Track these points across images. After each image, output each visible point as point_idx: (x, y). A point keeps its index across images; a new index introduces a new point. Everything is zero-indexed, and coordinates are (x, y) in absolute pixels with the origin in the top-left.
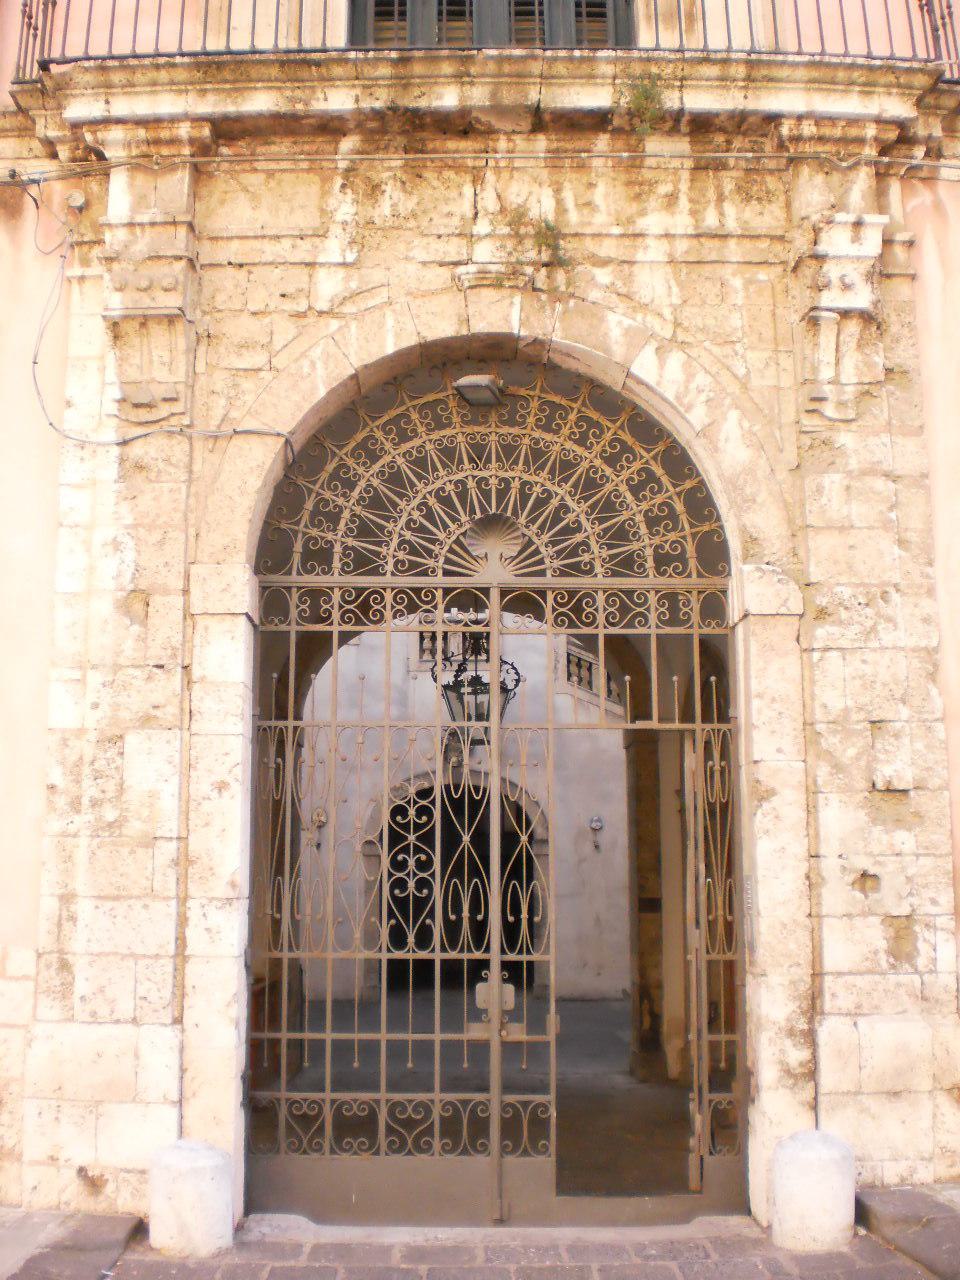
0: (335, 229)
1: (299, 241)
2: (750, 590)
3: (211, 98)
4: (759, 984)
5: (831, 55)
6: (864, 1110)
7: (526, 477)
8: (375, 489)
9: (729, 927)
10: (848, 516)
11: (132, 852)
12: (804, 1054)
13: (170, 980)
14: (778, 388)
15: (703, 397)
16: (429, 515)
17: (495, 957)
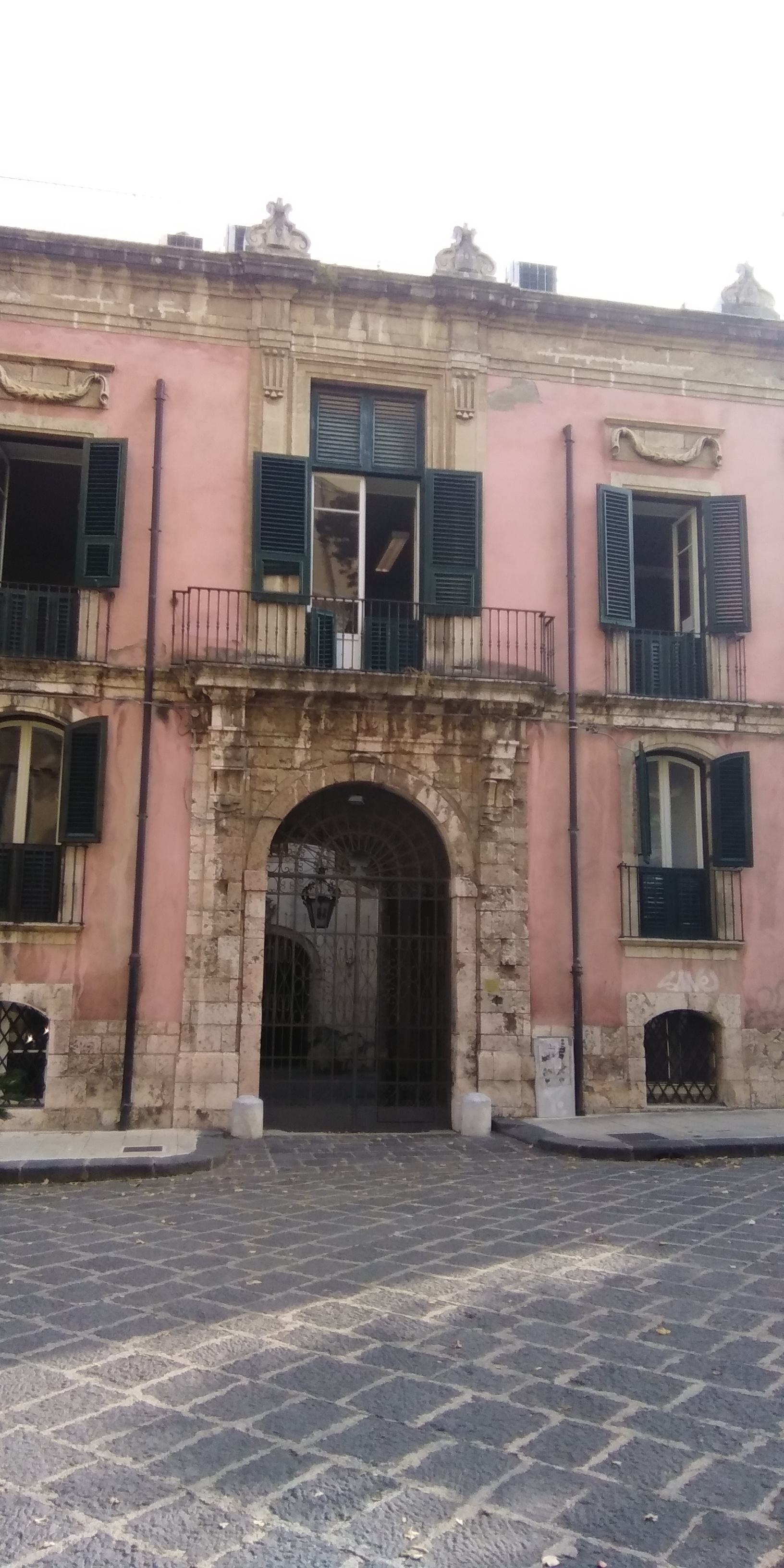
2: (459, 887)
6: (495, 1087)
12: (473, 1065)
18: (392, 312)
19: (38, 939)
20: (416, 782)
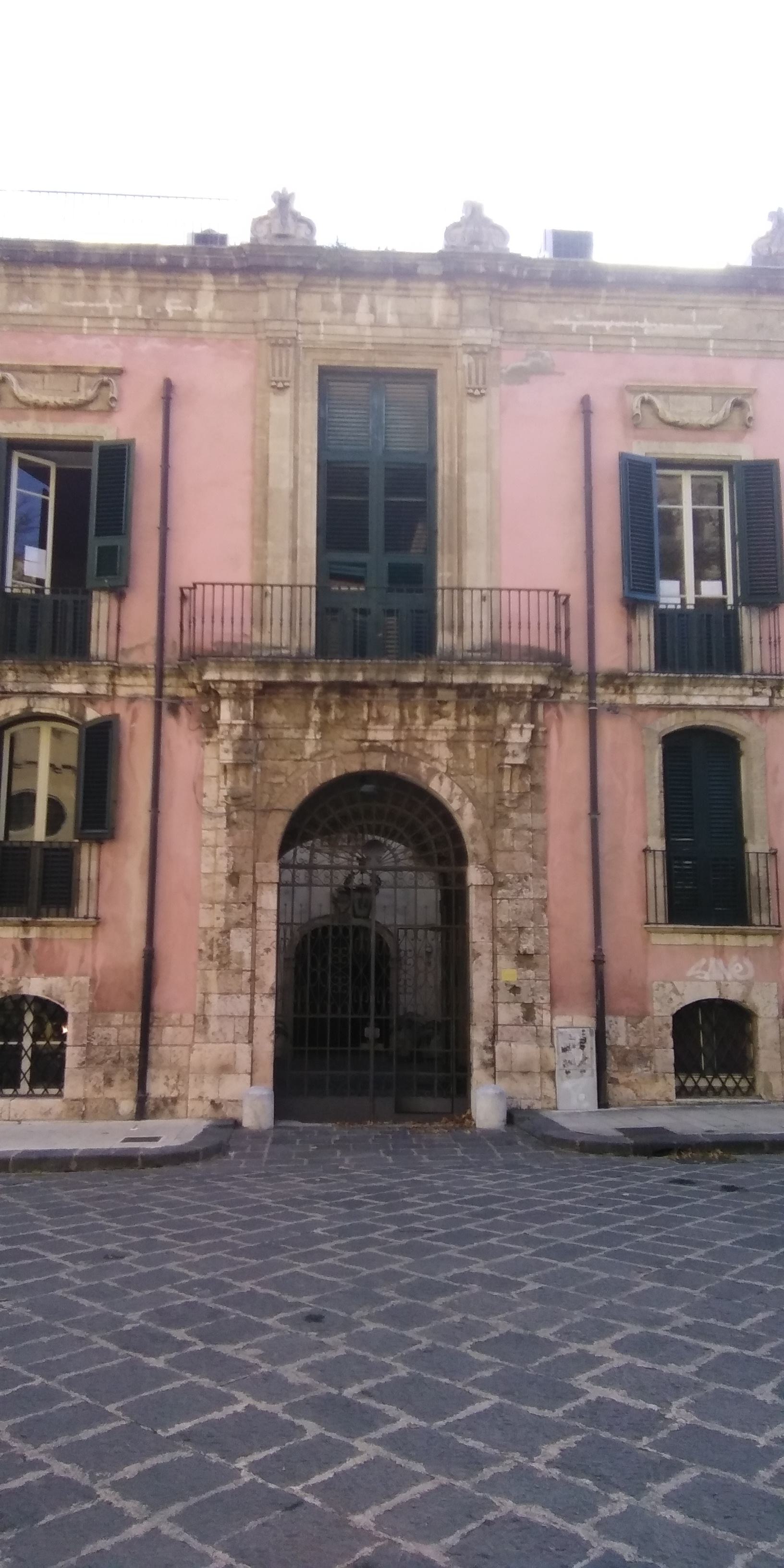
2: (474, 875)
15: (458, 797)
18: (400, 292)
19: (55, 933)
20: (428, 770)
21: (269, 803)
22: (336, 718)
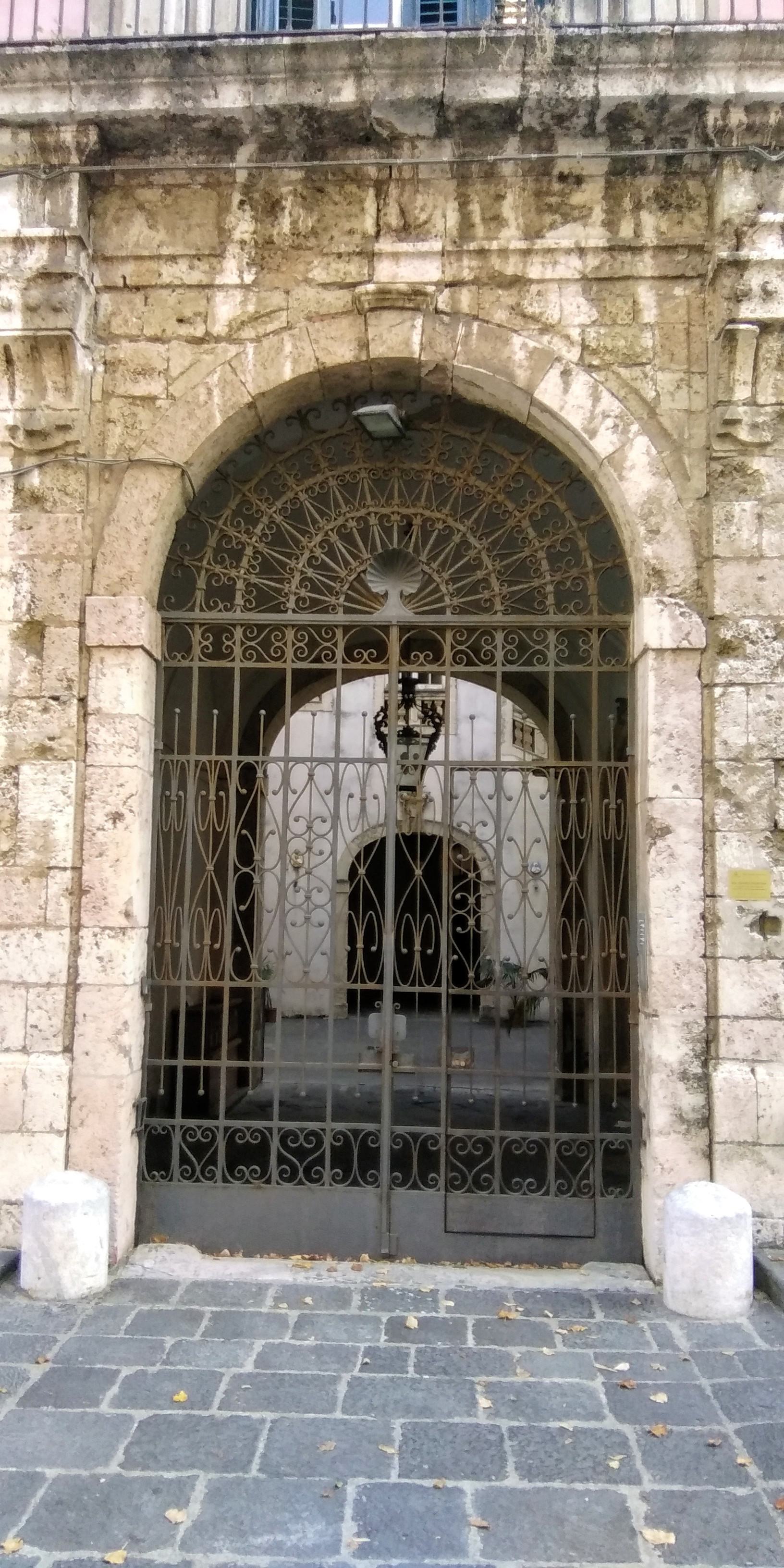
0: (233, 249)
1: (196, 262)
2: (654, 624)
3: (95, 95)
4: (651, 1025)
5: (767, 22)
6: (762, 1163)
7: (427, 513)
8: (278, 526)
9: (622, 965)
10: (759, 546)
11: (26, 881)
13: (61, 1007)
14: (689, 412)
15: (609, 422)
16: (331, 553)
17: (388, 988)
21: (122, 447)
22: (295, 233)
